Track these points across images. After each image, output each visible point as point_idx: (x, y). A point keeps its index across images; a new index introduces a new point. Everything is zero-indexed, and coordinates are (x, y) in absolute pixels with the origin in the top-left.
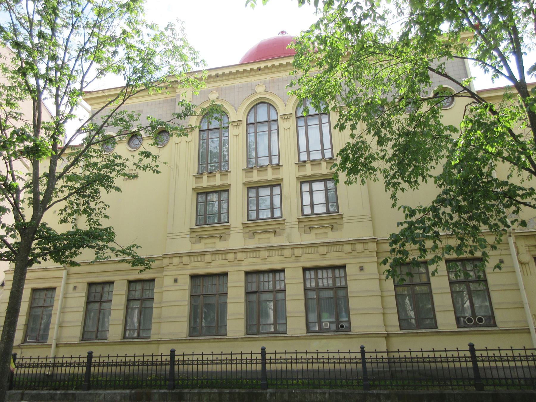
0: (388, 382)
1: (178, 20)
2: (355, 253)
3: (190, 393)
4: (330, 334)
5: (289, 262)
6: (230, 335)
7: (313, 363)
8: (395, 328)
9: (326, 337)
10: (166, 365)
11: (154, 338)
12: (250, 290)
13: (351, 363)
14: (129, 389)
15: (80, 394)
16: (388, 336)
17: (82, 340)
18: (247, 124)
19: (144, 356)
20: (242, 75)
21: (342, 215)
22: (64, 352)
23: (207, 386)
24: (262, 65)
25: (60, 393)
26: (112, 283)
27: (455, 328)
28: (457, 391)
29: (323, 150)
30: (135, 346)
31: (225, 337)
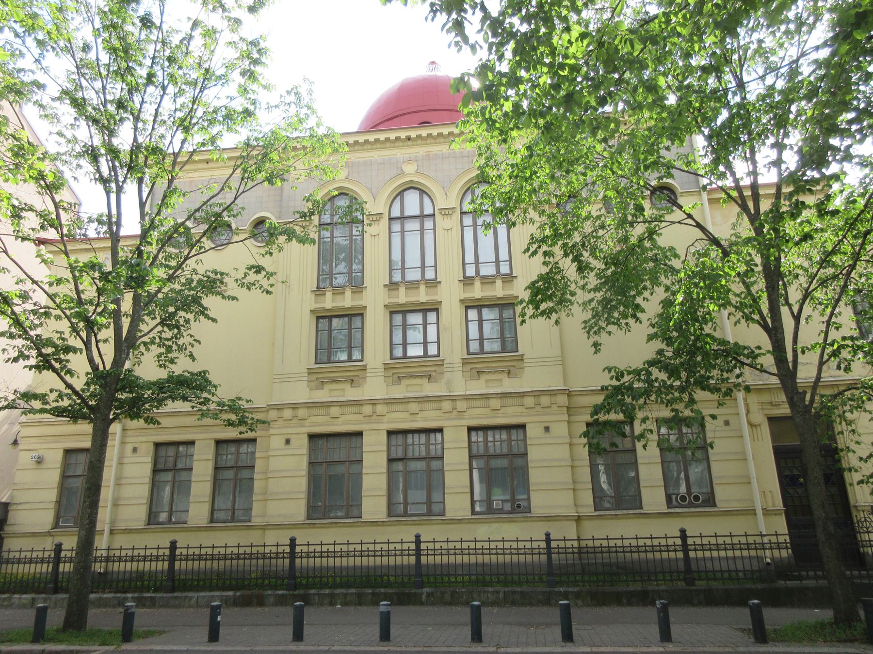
0: (579, 578)
1: (305, 80)
2: (538, 408)
3: (318, 594)
4: (503, 516)
5: (449, 419)
6: (366, 517)
7: (483, 554)
8: (588, 509)
9: (497, 521)
10: (284, 558)
11: (256, 521)
12: (393, 456)
13: (532, 554)
14: (231, 590)
15: (161, 598)
16: (579, 519)
17: (148, 524)
18: (390, 219)
19: (277, 546)
20: (383, 146)
21: (522, 355)
22: (121, 541)
23: (341, 586)
24: (413, 134)
25: (132, 597)
26: (192, 443)
27: (665, 509)
28: (663, 588)
29: (497, 262)
30: (229, 532)
31: (360, 520)
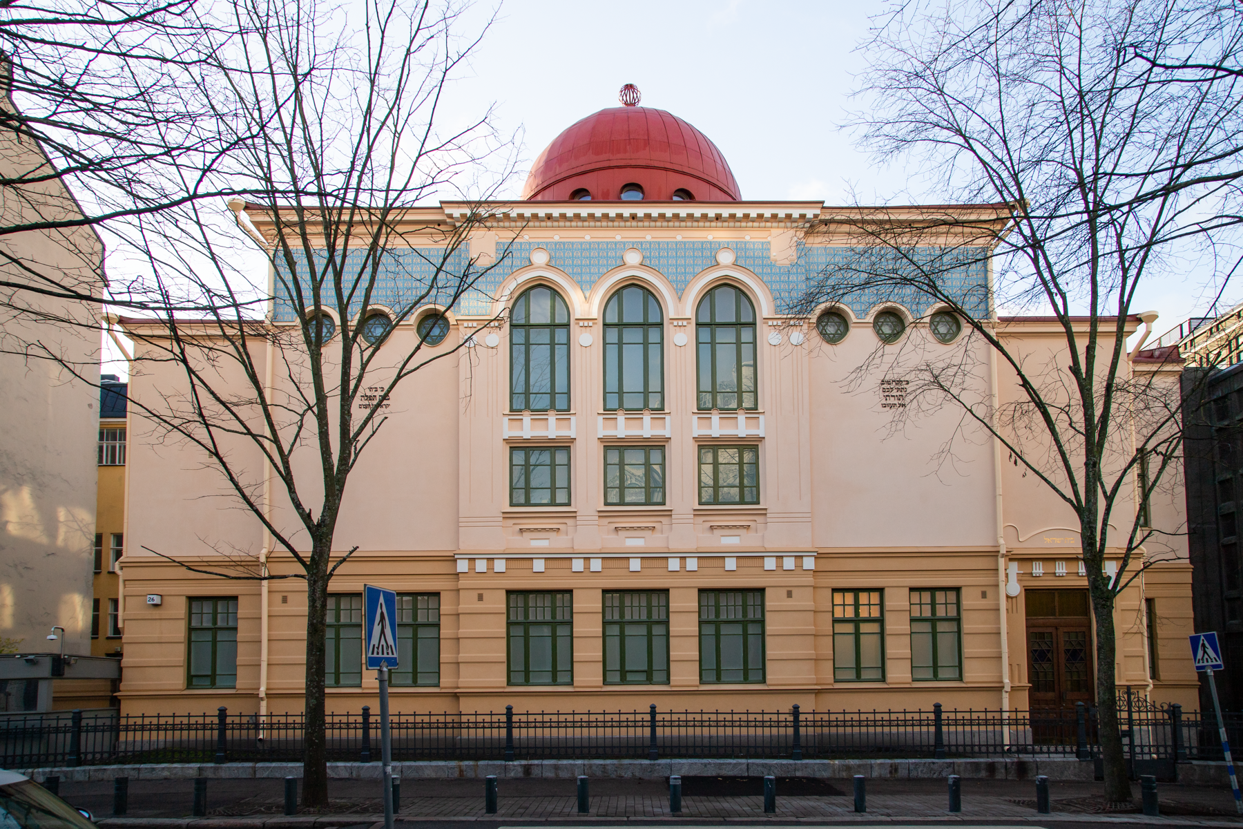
18: (605, 325)
